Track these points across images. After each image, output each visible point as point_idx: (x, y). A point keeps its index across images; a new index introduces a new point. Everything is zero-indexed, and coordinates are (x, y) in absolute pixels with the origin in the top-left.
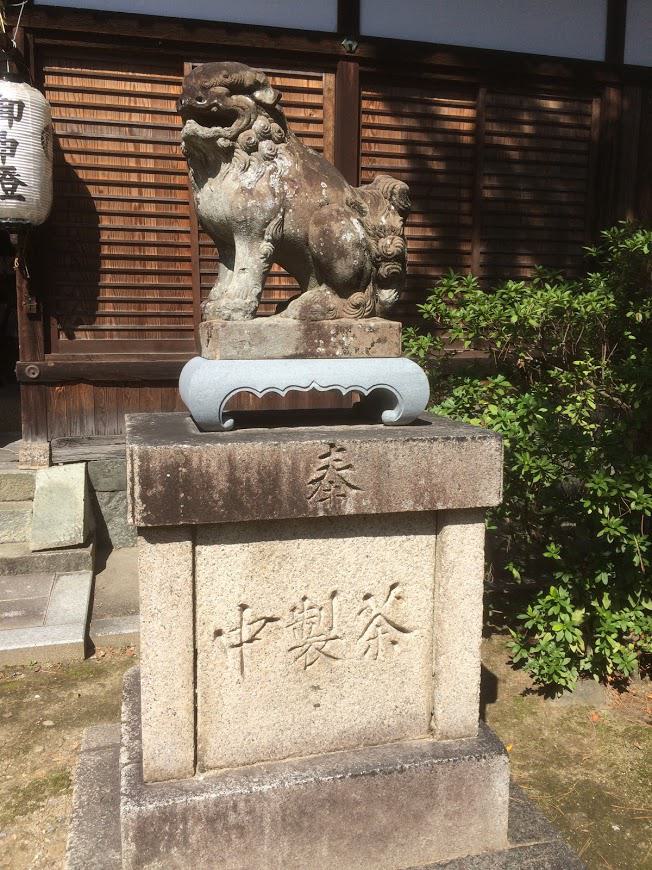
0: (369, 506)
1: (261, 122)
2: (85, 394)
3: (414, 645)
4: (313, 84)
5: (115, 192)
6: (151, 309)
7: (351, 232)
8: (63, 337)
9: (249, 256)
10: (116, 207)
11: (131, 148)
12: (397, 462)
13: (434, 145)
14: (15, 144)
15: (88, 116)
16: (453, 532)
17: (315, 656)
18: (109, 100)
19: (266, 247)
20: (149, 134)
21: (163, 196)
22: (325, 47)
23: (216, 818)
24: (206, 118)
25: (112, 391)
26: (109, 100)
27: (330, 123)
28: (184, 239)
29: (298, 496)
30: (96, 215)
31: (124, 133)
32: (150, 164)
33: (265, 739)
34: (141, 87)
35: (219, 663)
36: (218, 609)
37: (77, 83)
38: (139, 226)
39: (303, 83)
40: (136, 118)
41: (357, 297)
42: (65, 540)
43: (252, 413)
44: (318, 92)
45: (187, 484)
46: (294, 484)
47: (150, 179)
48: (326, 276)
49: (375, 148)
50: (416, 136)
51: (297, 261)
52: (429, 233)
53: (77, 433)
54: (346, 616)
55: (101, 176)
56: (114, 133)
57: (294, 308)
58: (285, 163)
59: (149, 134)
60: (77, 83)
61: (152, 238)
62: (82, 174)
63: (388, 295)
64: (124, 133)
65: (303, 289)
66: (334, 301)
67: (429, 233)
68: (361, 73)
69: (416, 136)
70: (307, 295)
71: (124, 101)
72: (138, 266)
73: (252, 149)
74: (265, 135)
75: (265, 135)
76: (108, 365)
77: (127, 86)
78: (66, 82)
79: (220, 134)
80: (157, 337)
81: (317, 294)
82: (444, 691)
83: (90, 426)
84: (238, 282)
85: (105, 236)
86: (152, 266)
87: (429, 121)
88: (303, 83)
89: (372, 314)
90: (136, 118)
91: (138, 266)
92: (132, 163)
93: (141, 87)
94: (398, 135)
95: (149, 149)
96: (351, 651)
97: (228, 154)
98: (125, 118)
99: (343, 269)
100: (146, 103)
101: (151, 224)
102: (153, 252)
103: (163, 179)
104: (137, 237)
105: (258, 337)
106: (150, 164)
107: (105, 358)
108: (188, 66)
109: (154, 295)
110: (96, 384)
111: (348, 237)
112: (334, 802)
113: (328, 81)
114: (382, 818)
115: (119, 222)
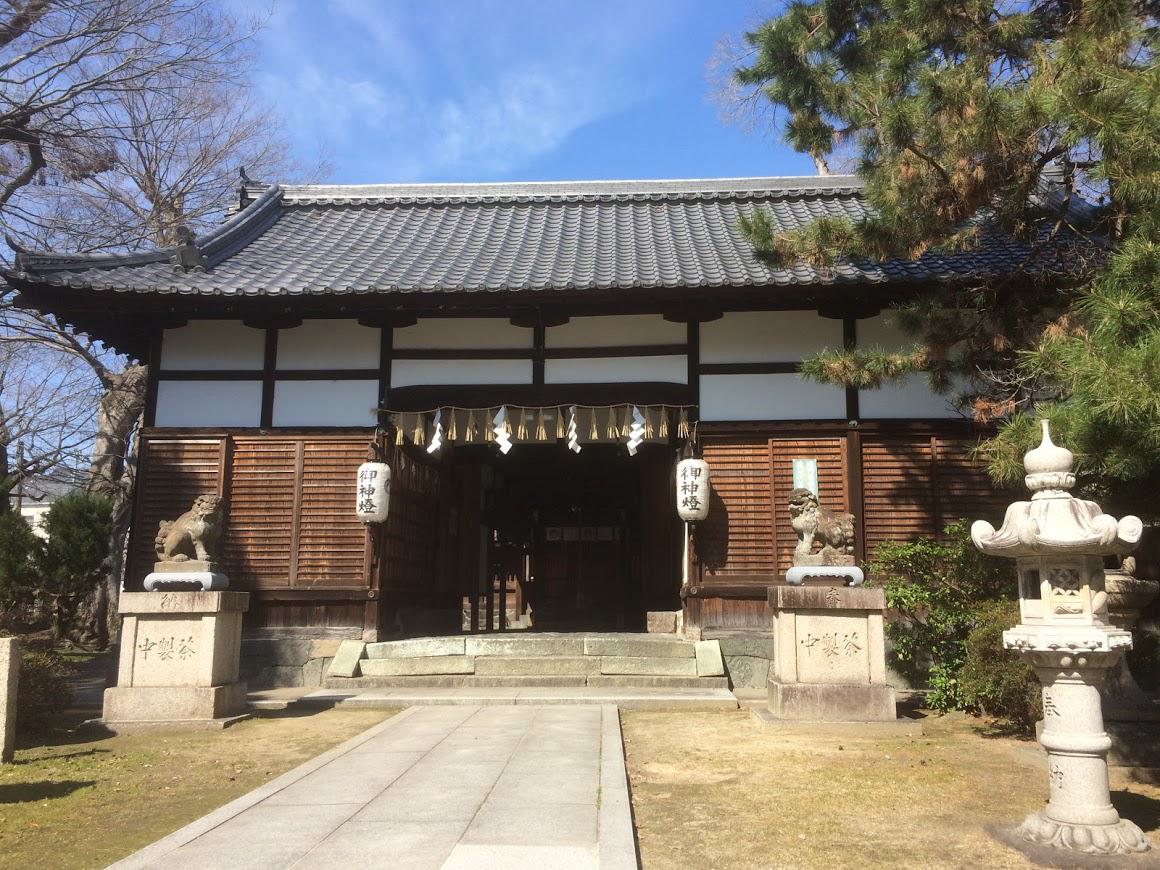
0: (844, 606)
1: (810, 504)
2: (718, 602)
3: (862, 654)
4: (835, 443)
5: (735, 501)
6: (751, 559)
7: (837, 531)
8: (708, 573)
9: (808, 538)
10: (734, 508)
11: (742, 480)
12: (855, 596)
13: (920, 468)
14: (697, 486)
15: (722, 467)
16: (872, 617)
17: (831, 652)
18: (732, 459)
19: (813, 535)
20: (751, 473)
21: (758, 502)
22: (842, 427)
23: (804, 692)
24: (796, 504)
25: (731, 602)
26: (732, 459)
27: (845, 461)
28: (768, 523)
29: (823, 603)
30: (726, 513)
31: (739, 473)
32: (751, 487)
33: (817, 676)
34: (747, 452)
35: (803, 650)
36: (802, 635)
37: (718, 452)
38: (745, 517)
39: (830, 443)
40: (745, 466)
41: (840, 549)
42: (716, 672)
43: (807, 579)
44: (838, 447)
45: (794, 597)
46: (822, 599)
47: (751, 494)
48: (830, 543)
49: (872, 472)
50: (907, 464)
51: (821, 539)
52: (924, 515)
53: (714, 624)
54: (841, 642)
55: (728, 494)
56: (734, 474)
57: (821, 552)
58: (817, 513)
59: (751, 473)
60: (718, 452)
61: (752, 523)
62: (719, 494)
63: (850, 548)
64: (739, 473)
65: (824, 546)
66: (833, 550)
67: (924, 515)
68: (861, 436)
69: (907, 464)
70: (825, 549)
71: (739, 459)
72: (745, 537)
73: (808, 510)
74: (812, 506)
75: (812, 506)
76: (731, 588)
77: (741, 452)
78: (713, 452)
79: (800, 507)
80: (755, 574)
81: (828, 548)
82: (873, 668)
83: (720, 621)
84: (804, 546)
85: (731, 523)
86: (752, 537)
87: (915, 457)
88: (830, 443)
89: (846, 554)
90: (745, 466)
91: (745, 537)
92: (743, 487)
93: (747, 452)
94: (896, 464)
95: (751, 480)
96: (842, 652)
97: (802, 512)
98: (739, 466)
99: (835, 541)
100: (750, 459)
101: (752, 516)
102: (752, 530)
103: (758, 494)
104: (745, 523)
105: (811, 560)
106: (751, 487)
107: (729, 585)
108: (770, 441)
109: (753, 552)
110: (724, 598)
111: (836, 532)
112: (838, 693)
113: (843, 441)
114: (854, 702)
115: (736, 516)
